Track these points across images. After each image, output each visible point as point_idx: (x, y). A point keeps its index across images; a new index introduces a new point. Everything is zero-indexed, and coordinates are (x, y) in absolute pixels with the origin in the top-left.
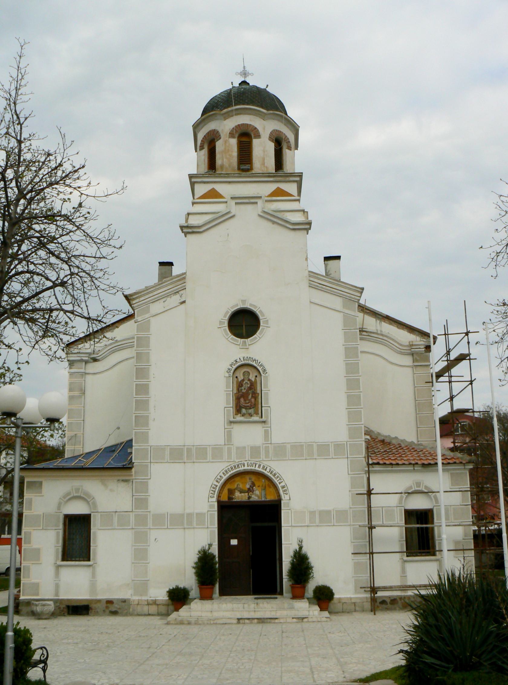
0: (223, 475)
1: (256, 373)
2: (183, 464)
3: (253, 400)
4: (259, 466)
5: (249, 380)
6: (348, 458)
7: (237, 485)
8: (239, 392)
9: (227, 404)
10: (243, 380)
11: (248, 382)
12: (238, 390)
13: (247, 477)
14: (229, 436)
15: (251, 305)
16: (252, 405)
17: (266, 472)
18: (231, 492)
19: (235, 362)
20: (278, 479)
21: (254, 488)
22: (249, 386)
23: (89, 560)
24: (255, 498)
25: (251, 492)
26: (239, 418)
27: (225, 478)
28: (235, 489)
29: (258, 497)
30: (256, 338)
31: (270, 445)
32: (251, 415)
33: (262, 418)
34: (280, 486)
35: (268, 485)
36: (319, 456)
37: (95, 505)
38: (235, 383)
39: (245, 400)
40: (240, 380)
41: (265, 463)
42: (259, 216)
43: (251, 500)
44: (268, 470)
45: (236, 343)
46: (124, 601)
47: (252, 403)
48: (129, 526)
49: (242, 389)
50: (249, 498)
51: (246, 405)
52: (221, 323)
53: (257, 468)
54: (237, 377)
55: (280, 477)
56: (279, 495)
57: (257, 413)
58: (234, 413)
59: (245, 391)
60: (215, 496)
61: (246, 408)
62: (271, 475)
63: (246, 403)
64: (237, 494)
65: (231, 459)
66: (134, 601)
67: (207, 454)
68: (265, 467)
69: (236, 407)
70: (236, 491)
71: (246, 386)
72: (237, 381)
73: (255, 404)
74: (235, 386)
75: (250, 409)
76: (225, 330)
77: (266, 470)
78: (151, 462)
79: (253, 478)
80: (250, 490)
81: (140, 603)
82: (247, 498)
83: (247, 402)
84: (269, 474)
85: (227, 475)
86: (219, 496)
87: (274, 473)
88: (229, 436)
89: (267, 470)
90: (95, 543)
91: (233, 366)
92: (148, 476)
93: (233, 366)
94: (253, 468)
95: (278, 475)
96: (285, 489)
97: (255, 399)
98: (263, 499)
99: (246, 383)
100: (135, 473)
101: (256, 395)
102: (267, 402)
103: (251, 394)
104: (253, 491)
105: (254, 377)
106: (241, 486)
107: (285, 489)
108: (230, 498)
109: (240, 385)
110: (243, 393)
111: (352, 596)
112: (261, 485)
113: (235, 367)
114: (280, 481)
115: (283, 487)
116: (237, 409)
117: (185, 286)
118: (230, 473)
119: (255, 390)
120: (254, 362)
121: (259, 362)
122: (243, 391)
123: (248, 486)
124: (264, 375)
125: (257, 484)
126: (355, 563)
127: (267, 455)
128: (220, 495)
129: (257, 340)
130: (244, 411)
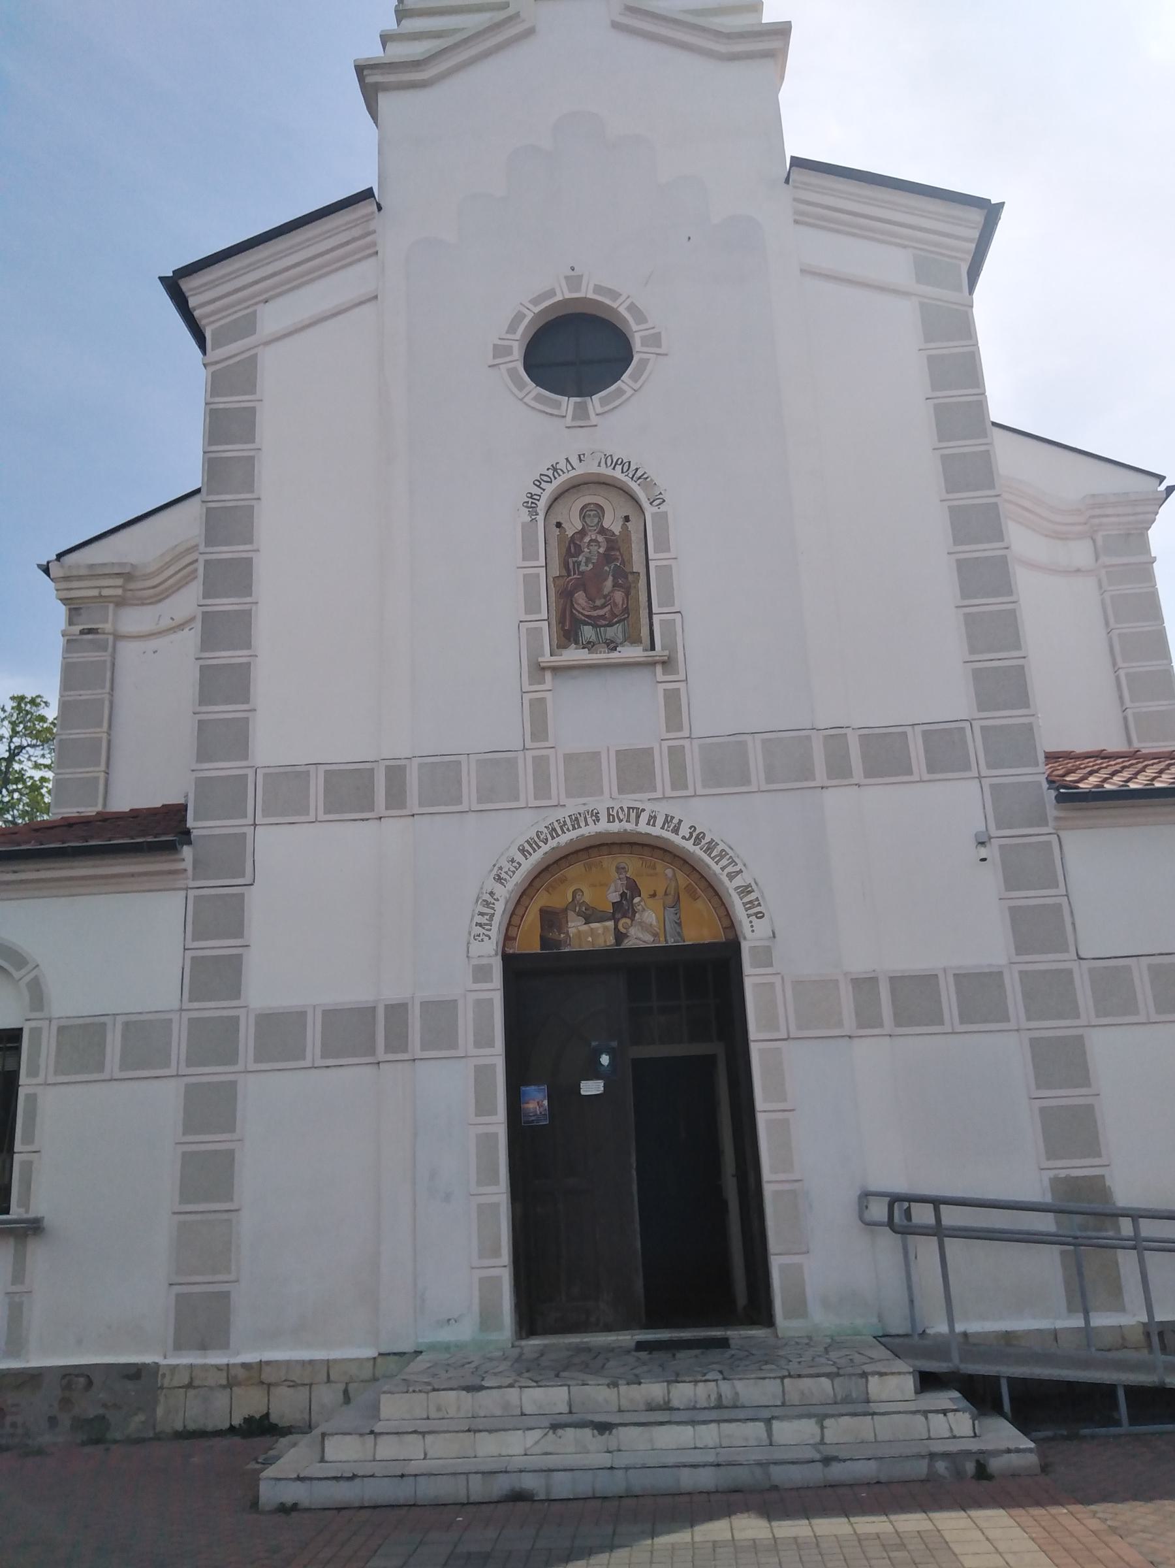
0: (519, 857)
1: (628, 510)
2: (377, 822)
3: (619, 596)
4: (652, 820)
5: (603, 531)
6: (980, 777)
7: (574, 897)
8: (569, 575)
9: (528, 611)
10: (582, 533)
11: (600, 539)
12: (566, 565)
13: (609, 863)
14: (539, 726)
15: (598, 289)
16: (616, 611)
17: (676, 839)
18: (551, 919)
19: (550, 473)
20: (724, 862)
21: (637, 900)
22: (601, 550)
23: (407, 1004)
24: (639, 937)
25: (624, 916)
26: (574, 655)
27: (528, 864)
28: (565, 910)
29: (655, 935)
30: (620, 392)
31: (686, 743)
32: (612, 646)
33: (653, 648)
34: (730, 887)
35: (689, 889)
36: (868, 775)
37: (37, 996)
38: (554, 543)
39: (590, 599)
40: (570, 533)
41: (676, 810)
42: (615, 25)
43: (627, 944)
44: (684, 830)
45: (555, 412)
46: (135, 1373)
47: (616, 604)
48: (167, 1065)
49: (579, 564)
50: (620, 936)
51: (595, 613)
52: (500, 351)
53: (643, 827)
54: (559, 525)
55: (731, 853)
56: (731, 925)
57: (635, 640)
58: (555, 642)
59: (591, 566)
60: (494, 933)
61: (594, 623)
62: (697, 851)
63: (596, 608)
64: (575, 926)
65: (550, 798)
66: (174, 1368)
67: (460, 782)
68: (675, 821)
69: (561, 621)
70: (571, 914)
71: (594, 548)
72: (561, 539)
73: (626, 610)
74: (555, 554)
75: (611, 625)
76: (512, 373)
77: (676, 831)
78: (255, 825)
79: (633, 864)
80: (623, 909)
81: (196, 1383)
82: (611, 940)
83: (598, 603)
84: (689, 845)
85: (537, 856)
86: (508, 938)
87: (707, 839)
88: (539, 726)
89: (681, 833)
90: (29, 1138)
91: (543, 485)
92: (243, 875)
93: (543, 485)
94: (630, 827)
95: (721, 846)
96: (752, 897)
97: (627, 594)
98: (671, 942)
99: (591, 540)
100: (194, 868)
101: (630, 578)
102: (669, 599)
103: (611, 578)
104: (634, 913)
105: (621, 522)
106: (588, 897)
107: (752, 897)
108: (545, 942)
109: (571, 548)
110: (582, 573)
111: (1060, 1324)
112: (660, 893)
113: (550, 489)
114: (730, 869)
115: (746, 890)
116: (563, 628)
117: (374, 244)
118: (545, 848)
119: (623, 562)
120: (619, 468)
121: (633, 467)
122: (583, 568)
123: (615, 897)
124: (655, 509)
125: (645, 886)
126: (251, 542)
127: (679, 779)
128: (512, 933)
129: (624, 397)
130: (588, 632)
